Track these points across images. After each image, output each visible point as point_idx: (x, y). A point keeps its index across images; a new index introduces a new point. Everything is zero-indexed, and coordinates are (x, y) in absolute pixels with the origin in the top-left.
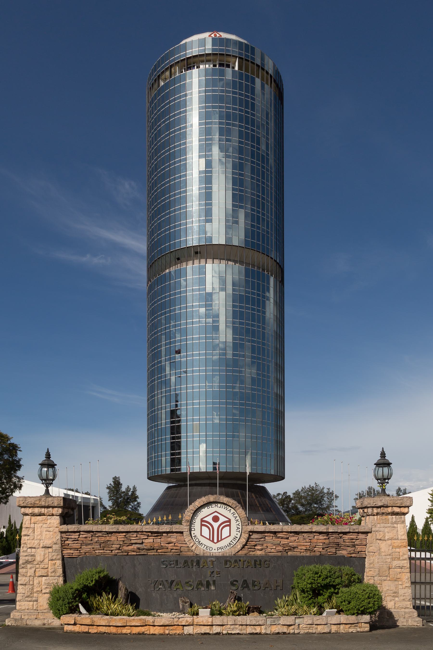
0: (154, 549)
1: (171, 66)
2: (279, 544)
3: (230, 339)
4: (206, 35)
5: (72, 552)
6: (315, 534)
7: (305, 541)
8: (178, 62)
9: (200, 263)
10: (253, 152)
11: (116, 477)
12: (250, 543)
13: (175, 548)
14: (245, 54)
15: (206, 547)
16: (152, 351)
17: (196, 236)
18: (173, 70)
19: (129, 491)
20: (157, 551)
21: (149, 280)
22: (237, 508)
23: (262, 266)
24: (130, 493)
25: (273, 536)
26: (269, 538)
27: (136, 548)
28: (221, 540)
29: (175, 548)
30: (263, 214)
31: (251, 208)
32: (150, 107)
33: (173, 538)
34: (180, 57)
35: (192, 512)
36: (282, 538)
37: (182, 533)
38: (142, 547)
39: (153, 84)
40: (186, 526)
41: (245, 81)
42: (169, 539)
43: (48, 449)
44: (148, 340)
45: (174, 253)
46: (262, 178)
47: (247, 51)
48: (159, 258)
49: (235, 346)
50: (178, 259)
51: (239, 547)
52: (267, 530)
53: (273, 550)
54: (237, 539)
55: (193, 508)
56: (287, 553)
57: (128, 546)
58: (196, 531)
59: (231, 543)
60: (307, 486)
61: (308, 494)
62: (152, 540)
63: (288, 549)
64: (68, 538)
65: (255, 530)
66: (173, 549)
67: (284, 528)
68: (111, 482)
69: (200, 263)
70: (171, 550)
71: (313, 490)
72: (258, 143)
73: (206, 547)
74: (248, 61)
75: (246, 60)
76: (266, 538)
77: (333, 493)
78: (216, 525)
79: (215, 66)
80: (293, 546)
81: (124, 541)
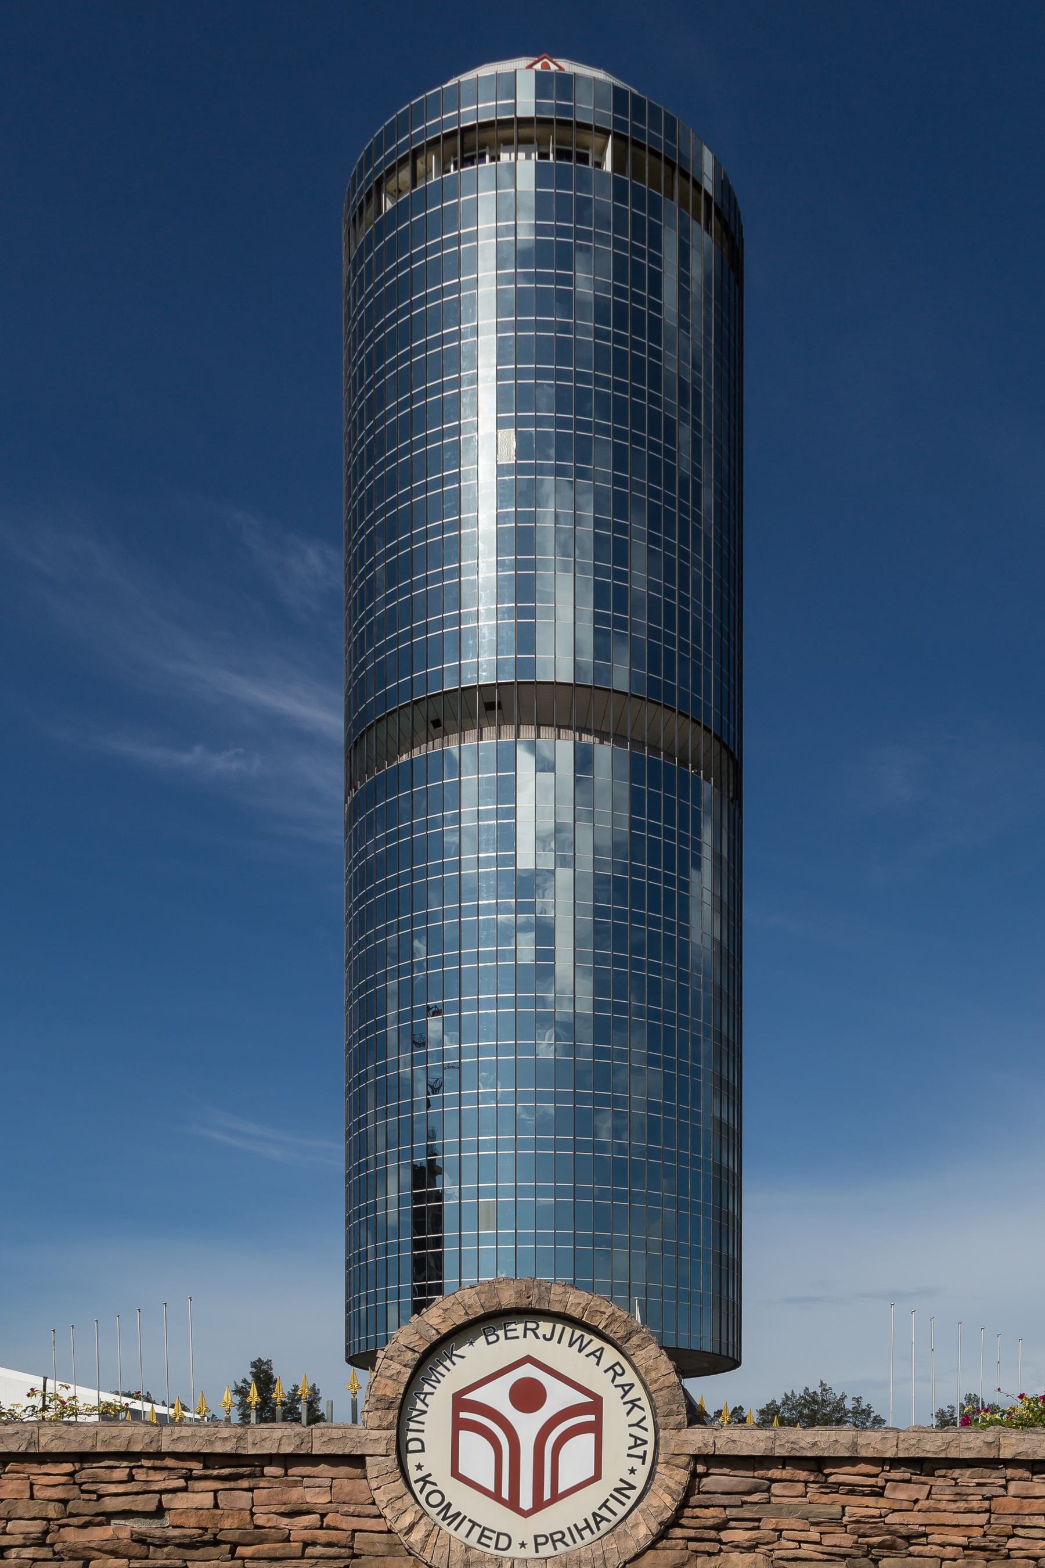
0: (216, 1543)
1: (416, 154)
2: (836, 1521)
3: (585, 1008)
4: (519, 64)
6: (1010, 1473)
7: (962, 1505)
8: (437, 139)
9: (499, 736)
10: (654, 463)
11: (260, 1360)
12: (698, 1512)
13: (323, 1536)
14: (633, 126)
15: (477, 1531)
16: (360, 991)
17: (487, 658)
18: (420, 166)
19: (299, 1400)
20: (232, 1552)
21: (351, 785)
22: (635, 1340)
23: (679, 752)
25: (806, 1482)
26: (790, 1492)
27: (125, 1534)
28: (556, 1497)
29: (323, 1536)
30: (684, 600)
31: (632, 820)
32: (355, 275)
33: (314, 1490)
34: (442, 124)
35: (410, 1357)
36: (852, 1490)
37: (357, 1461)
38: (158, 1533)
39: (361, 207)
40: (379, 1428)
41: (633, 206)
42: (295, 1495)
44: (349, 959)
45: (423, 706)
46: (680, 496)
47: (638, 116)
48: (378, 721)
49: (601, 1029)
50: (437, 723)
51: (643, 1531)
52: (780, 1452)
53: (807, 1550)
54: (634, 1495)
55: (414, 1340)
56: (876, 1561)
57: (84, 1526)
58: (430, 1457)
59: (604, 1512)
60: (799, 1392)
61: (801, 1412)
62: (207, 1499)
63: (881, 1545)
65: (723, 1449)
66: (314, 1544)
67: (861, 1441)
69: (499, 736)
70: (306, 1544)
71: (815, 1402)
72: (670, 438)
73: (477, 1531)
74: (642, 146)
75: (635, 143)
76: (776, 1489)
77: (869, 1413)
78: (527, 1426)
79: (544, 156)
80: (903, 1531)
81: (65, 1502)
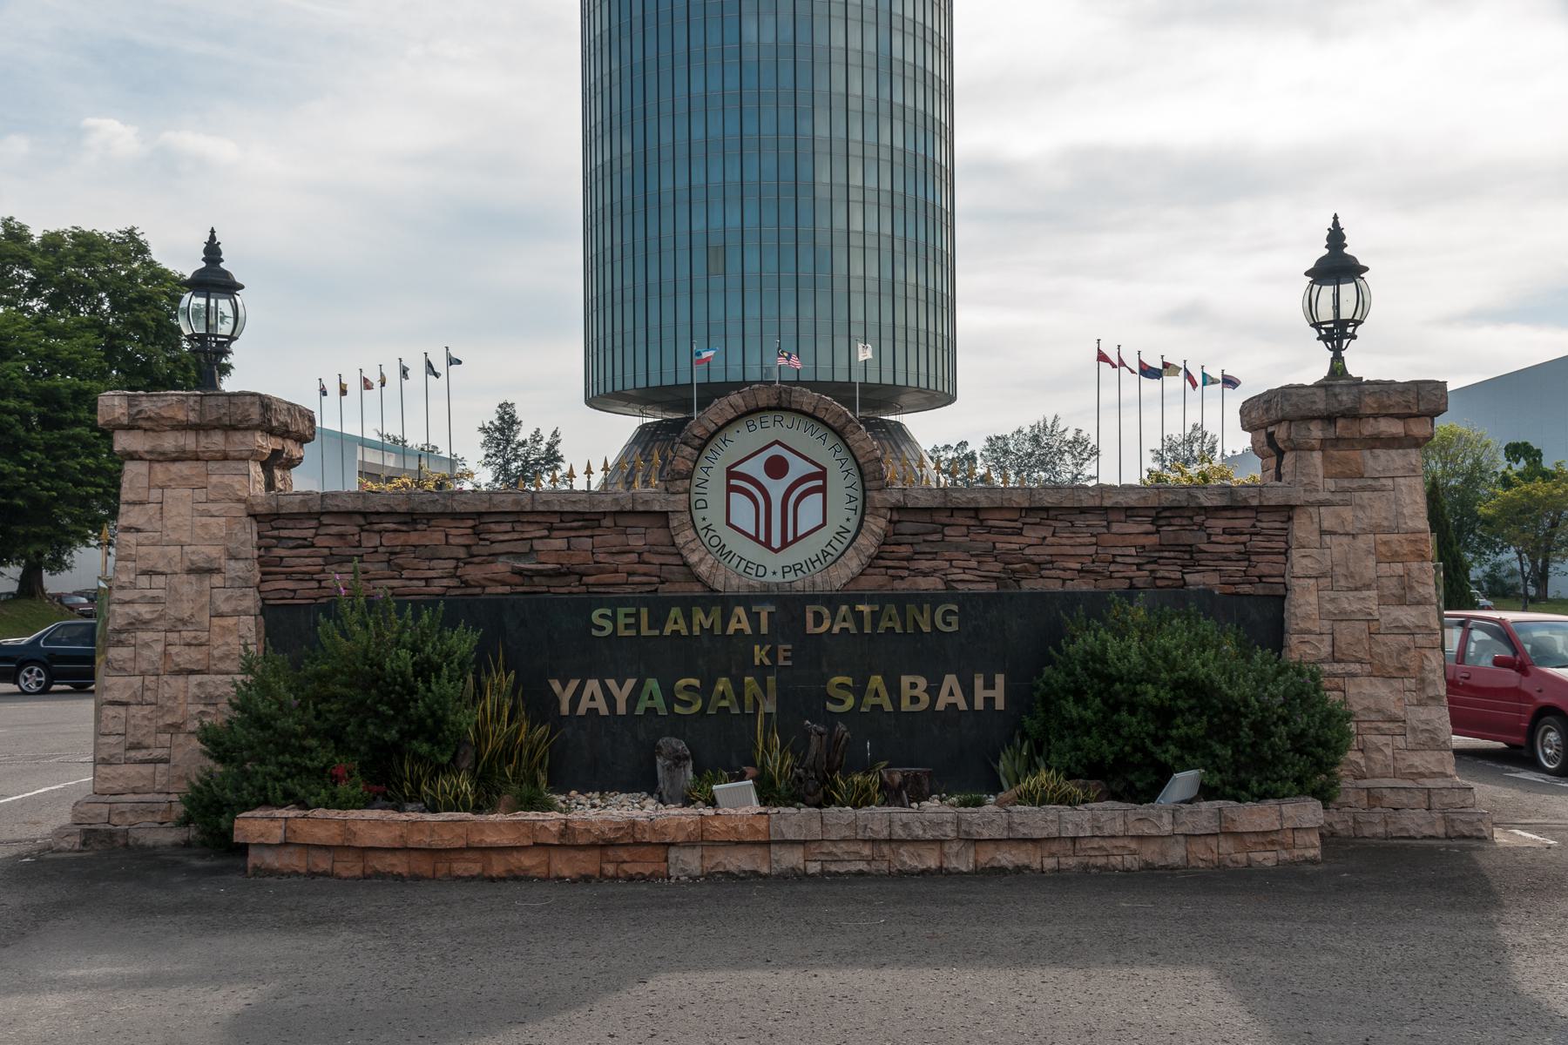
5: (290, 585)
24: (543, 447)
28: (796, 539)
36: (1001, 531)
43: (213, 231)
54: (849, 536)
56: (1018, 582)
59: (829, 549)
64: (279, 538)
68: (491, 417)
70: (629, 574)
73: (743, 563)
78: (776, 489)
80: (1037, 559)
81: (467, 546)
